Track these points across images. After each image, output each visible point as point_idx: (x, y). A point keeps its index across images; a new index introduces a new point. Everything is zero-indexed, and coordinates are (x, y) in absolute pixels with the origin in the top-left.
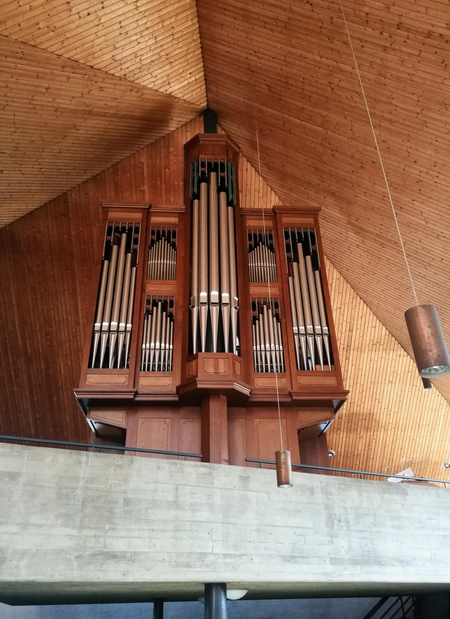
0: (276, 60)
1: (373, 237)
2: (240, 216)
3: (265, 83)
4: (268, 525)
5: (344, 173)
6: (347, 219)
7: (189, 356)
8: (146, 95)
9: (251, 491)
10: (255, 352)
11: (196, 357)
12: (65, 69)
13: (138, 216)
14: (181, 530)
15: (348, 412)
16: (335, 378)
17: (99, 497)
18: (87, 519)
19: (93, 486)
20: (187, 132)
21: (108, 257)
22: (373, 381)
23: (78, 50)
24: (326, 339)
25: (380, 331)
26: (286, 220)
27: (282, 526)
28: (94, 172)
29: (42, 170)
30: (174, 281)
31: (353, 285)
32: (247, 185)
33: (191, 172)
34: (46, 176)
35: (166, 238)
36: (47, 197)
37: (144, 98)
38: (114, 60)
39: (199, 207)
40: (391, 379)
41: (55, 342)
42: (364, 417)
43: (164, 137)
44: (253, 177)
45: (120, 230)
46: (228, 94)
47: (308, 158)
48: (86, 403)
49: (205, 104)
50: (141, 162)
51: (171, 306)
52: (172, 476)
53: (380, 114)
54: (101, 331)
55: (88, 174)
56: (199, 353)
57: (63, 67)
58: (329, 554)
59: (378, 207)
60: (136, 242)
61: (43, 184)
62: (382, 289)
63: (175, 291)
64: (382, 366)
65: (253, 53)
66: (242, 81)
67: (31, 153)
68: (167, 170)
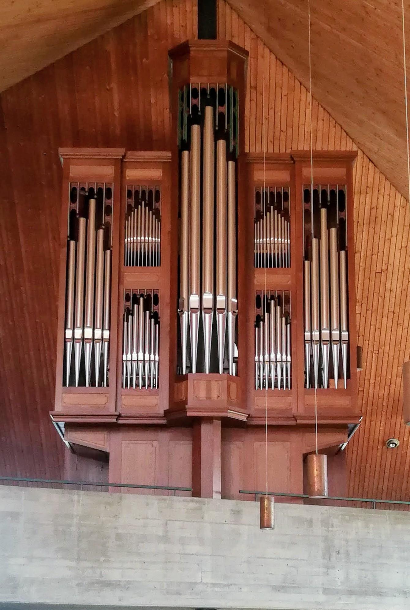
7: (178, 378)
9: (242, 524)
11: (185, 378)
20: (173, 6)
24: (344, 347)
35: (147, 202)
43: (139, 16)
58: (323, 584)
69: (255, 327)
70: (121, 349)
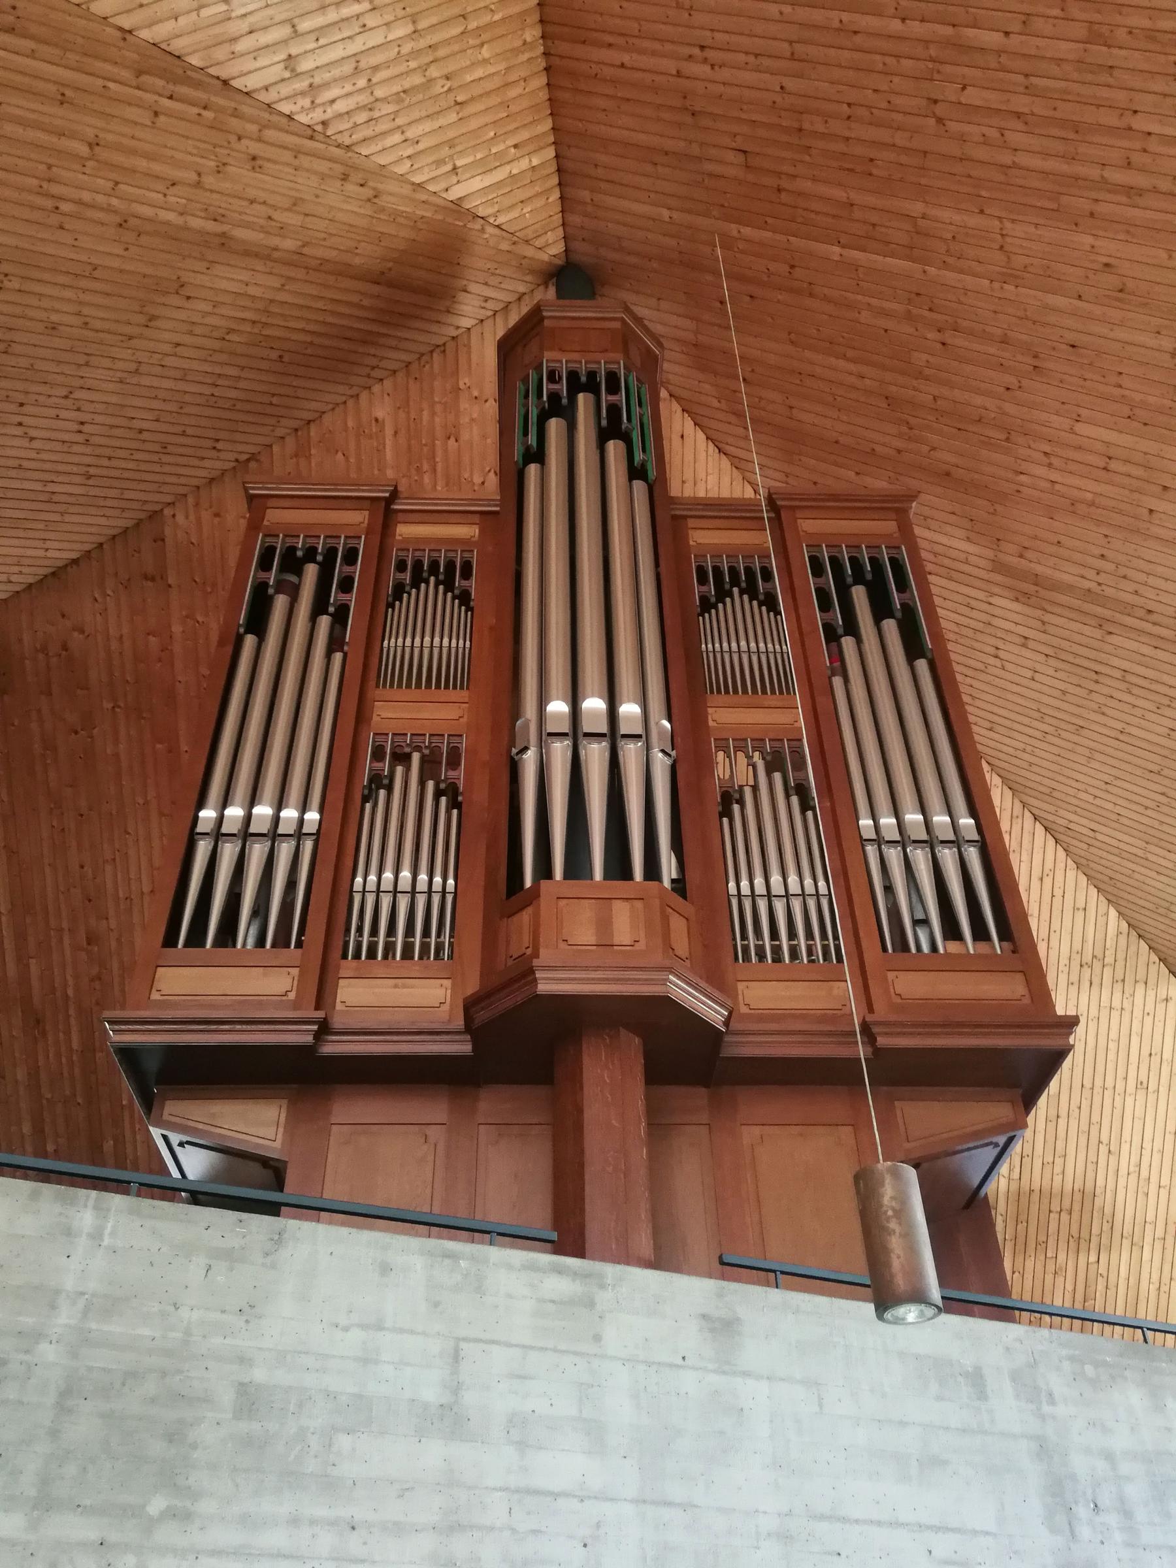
0: (766, 62)
1: (1076, 603)
2: (668, 519)
3: (734, 145)
4: (822, 1517)
5: (978, 400)
6: (990, 554)
8: (390, 198)
9: (746, 1374)
10: (734, 902)
12: (145, 78)
13: (358, 518)
14: (472, 1527)
15: (1014, 1186)
16: (1019, 977)
17: (132, 1375)
18: (71, 1469)
19: (115, 1328)
21: (257, 623)
22: (1088, 1084)
23: (182, 21)
24: (973, 855)
25: (1101, 920)
26: (809, 525)
27: (879, 1523)
28: (241, 448)
29: (86, 428)
30: (465, 693)
31: (1012, 777)
32: (683, 482)
33: (519, 400)
34: (99, 451)
36: (103, 521)
37: (383, 210)
38: (293, 70)
39: (545, 486)
40: (1143, 1077)
41: (115, 965)
42: (1066, 1204)
44: (702, 456)
45: (300, 553)
46: (625, 204)
47: (864, 369)
48: (152, 1065)
49: (558, 248)
50: (377, 420)
51: (454, 763)
52: (436, 1304)
53: (1094, 172)
54: (218, 835)
55: (222, 455)
56: (544, 884)
57: (139, 73)
59: (1089, 496)
60: (346, 585)
61: (89, 477)
62: (1106, 778)
63: (464, 720)
64: (1113, 1035)
65: (696, 51)
66: (666, 153)
67: (52, 367)
68: (452, 441)
69: (721, 815)
70: (349, 862)
